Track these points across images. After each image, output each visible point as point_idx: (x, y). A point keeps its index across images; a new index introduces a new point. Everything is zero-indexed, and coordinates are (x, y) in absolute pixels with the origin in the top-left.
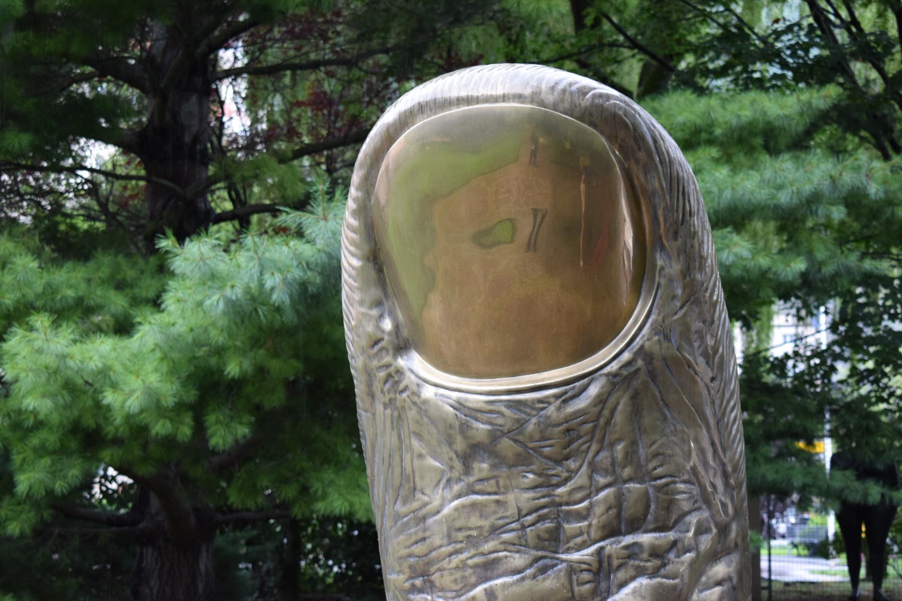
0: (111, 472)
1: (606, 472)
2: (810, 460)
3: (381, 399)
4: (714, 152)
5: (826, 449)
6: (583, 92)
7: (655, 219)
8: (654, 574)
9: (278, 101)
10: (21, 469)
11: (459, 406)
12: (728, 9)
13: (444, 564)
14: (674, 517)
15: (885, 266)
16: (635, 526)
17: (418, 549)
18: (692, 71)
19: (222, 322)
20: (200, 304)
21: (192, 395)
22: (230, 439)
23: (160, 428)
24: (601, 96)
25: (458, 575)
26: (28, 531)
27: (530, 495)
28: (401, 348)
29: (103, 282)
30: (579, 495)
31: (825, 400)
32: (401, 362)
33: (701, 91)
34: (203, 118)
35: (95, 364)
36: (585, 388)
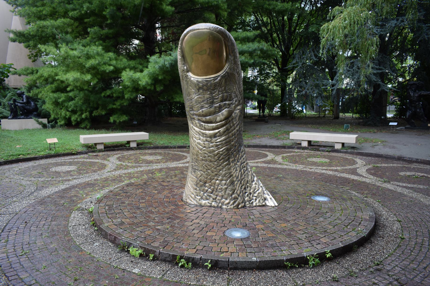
0: (141, 96)
1: (221, 92)
2: (253, 93)
3: (184, 80)
4: (239, 42)
5: (256, 92)
6: (217, 28)
7: (229, 50)
8: (228, 108)
9: (166, 33)
10: (126, 94)
11: (197, 81)
12: (242, 18)
13: (195, 107)
14: (232, 99)
15: (266, 61)
16: (225, 101)
17: (191, 104)
18: (236, 28)
19: (158, 70)
20: (154, 67)
21: (153, 82)
22: (160, 89)
23: (148, 88)
24: (220, 29)
25: (197, 108)
26: (127, 104)
27: (209, 95)
28: (188, 71)
29: (138, 64)
30: (216, 95)
31: (256, 84)
32: (188, 74)
33: (237, 32)
34: (154, 35)
35: (137, 77)
36: (218, 78)
